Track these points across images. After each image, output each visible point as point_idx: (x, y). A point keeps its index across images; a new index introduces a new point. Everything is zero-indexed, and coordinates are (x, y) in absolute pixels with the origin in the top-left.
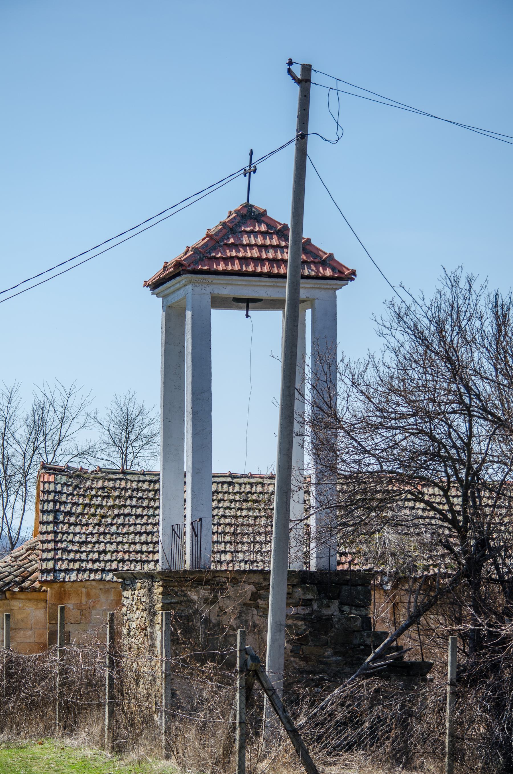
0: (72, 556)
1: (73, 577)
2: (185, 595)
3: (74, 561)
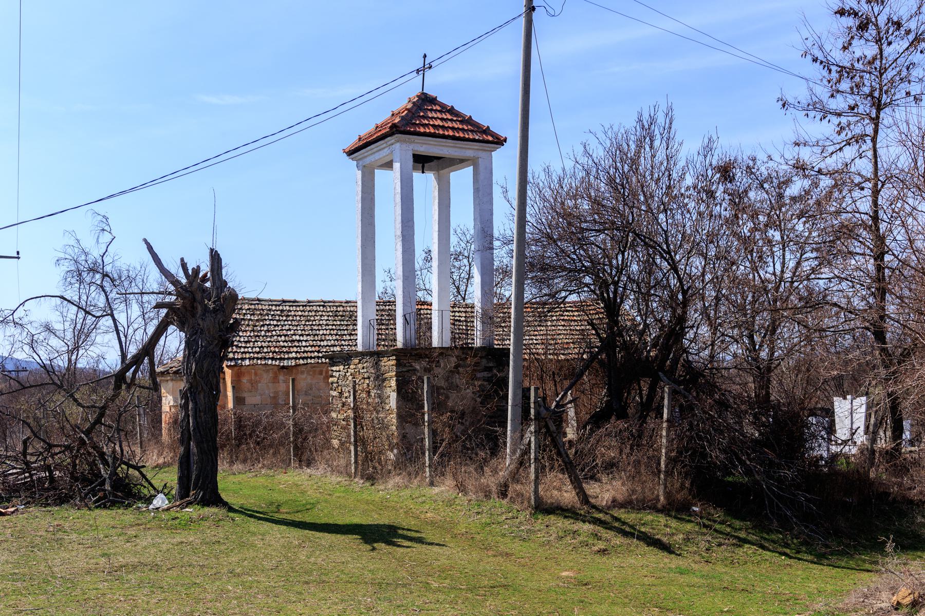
0: (242, 350)
1: (247, 362)
2: (411, 366)
3: (245, 353)
